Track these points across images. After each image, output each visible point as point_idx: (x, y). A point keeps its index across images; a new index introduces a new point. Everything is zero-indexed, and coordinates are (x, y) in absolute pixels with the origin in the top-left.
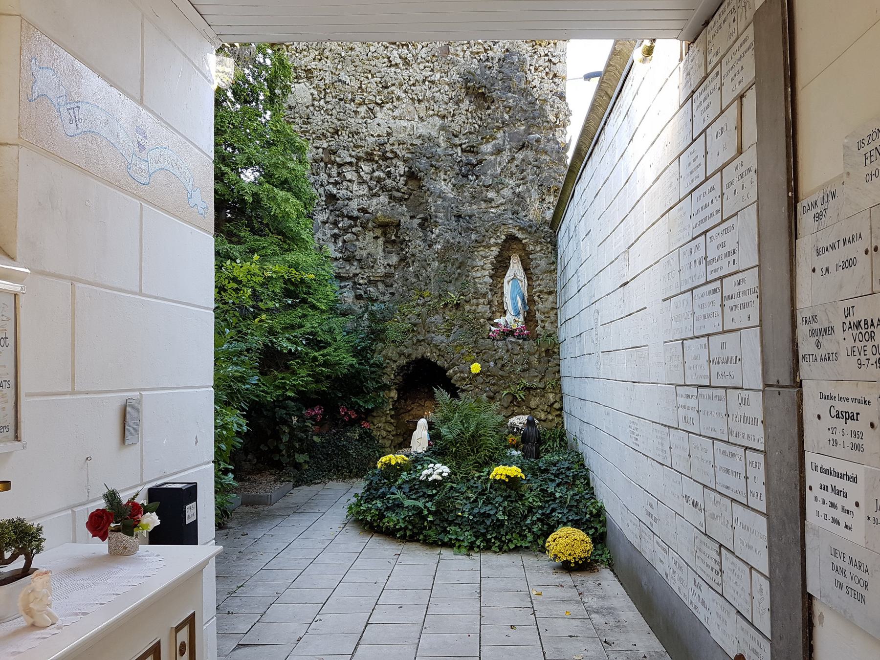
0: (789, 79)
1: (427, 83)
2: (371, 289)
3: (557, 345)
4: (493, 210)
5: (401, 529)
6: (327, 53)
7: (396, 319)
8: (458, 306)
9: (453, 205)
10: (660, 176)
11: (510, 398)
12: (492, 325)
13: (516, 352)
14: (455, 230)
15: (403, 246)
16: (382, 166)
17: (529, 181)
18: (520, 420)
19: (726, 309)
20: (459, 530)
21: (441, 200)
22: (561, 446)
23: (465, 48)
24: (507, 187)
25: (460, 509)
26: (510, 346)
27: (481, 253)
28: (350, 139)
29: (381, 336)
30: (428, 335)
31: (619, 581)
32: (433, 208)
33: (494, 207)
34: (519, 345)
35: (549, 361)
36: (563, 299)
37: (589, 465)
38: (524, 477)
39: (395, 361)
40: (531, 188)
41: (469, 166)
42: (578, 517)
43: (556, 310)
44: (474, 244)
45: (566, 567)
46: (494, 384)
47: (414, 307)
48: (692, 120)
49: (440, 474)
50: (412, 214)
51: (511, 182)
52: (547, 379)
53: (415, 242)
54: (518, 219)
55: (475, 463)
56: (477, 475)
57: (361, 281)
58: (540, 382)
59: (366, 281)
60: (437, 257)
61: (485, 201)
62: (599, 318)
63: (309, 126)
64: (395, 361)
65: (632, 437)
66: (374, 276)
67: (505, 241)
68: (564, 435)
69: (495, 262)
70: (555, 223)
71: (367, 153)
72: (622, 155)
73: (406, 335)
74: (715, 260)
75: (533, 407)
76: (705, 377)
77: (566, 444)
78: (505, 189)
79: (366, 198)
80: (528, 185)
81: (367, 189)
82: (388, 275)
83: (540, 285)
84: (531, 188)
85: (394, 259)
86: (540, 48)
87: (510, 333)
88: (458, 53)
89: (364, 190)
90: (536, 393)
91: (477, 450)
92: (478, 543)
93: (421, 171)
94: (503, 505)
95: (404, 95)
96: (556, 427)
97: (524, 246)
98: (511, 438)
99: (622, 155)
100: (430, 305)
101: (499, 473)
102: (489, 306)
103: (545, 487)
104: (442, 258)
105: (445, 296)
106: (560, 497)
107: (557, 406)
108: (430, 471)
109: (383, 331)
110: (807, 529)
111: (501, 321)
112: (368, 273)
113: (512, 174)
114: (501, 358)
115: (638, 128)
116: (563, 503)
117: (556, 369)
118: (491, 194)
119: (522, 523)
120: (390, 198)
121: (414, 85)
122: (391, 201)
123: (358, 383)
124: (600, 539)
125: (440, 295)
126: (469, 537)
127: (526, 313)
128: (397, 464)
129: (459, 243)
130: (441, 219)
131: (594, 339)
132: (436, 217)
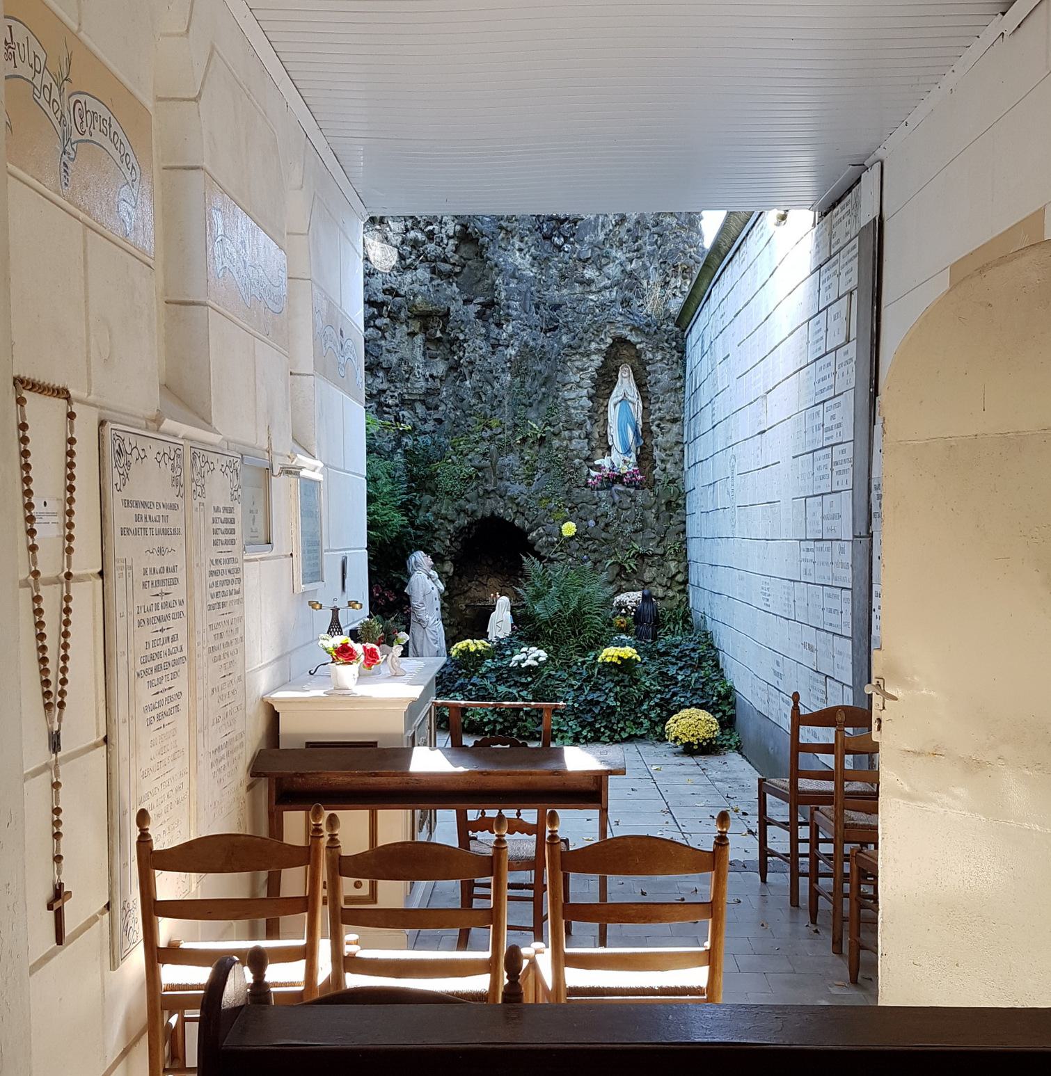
0: (875, 299)
2: (405, 413)
3: (682, 494)
4: (592, 297)
5: (489, 722)
7: (450, 460)
8: (542, 440)
9: (533, 288)
10: (794, 331)
11: (617, 569)
12: (591, 468)
13: (625, 506)
14: (536, 326)
15: (455, 348)
16: (419, 222)
17: (646, 254)
18: (631, 598)
19: (834, 472)
20: (562, 720)
21: (515, 281)
22: (684, 630)
24: (614, 261)
25: (561, 698)
26: (617, 498)
27: (577, 364)
29: (428, 485)
31: (748, 761)
32: (503, 294)
33: (594, 292)
34: (630, 496)
35: (671, 517)
36: (692, 432)
37: (719, 644)
38: (639, 660)
39: (452, 522)
40: (648, 264)
41: (554, 222)
42: (704, 701)
43: (681, 446)
44: (567, 351)
45: (689, 750)
46: (595, 551)
47: (477, 442)
48: (819, 291)
49: (536, 659)
50: (466, 297)
51: (619, 254)
52: (668, 542)
53: (473, 342)
54: (631, 313)
55: (577, 647)
56: (581, 660)
57: (390, 402)
58: (658, 546)
59: (397, 401)
60: (510, 368)
61: (581, 283)
62: (736, 466)
64: (452, 522)
65: (763, 598)
66: (409, 394)
67: (611, 346)
68: (689, 615)
69: (596, 376)
70: (685, 318)
72: (763, 285)
73: (468, 483)
74: (829, 429)
75: (648, 580)
76: (818, 532)
77: (691, 626)
78: (611, 265)
79: (395, 273)
80: (645, 259)
82: (429, 392)
83: (660, 409)
84: (648, 264)
85: (440, 368)
87: (618, 479)
90: (652, 562)
91: (579, 631)
92: (584, 733)
93: (483, 236)
94: (615, 690)
96: (679, 606)
97: (638, 354)
98: (618, 620)
99: (763, 285)
100: (500, 440)
101: (609, 654)
102: (587, 440)
103: (665, 670)
104: (518, 369)
105: (524, 426)
106: (682, 680)
107: (680, 578)
108: (524, 656)
109: (432, 476)
110: (872, 640)
111: (605, 462)
112: (401, 388)
113: (621, 242)
114: (605, 515)
115: (777, 267)
116: (685, 687)
118: (590, 273)
119: (637, 710)
120: (433, 272)
122: (434, 276)
123: (398, 552)
124: (728, 723)
125: (516, 425)
126: (574, 727)
127: (639, 450)
128: (477, 651)
129: (543, 347)
130: (516, 310)
131: (730, 491)
132: (509, 307)
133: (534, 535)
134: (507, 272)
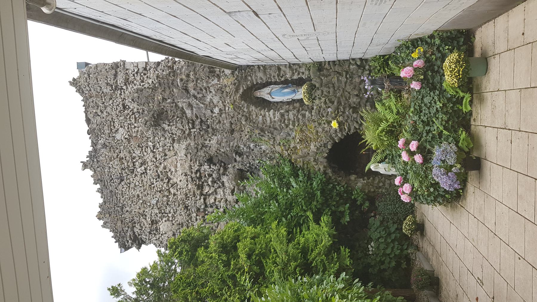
1: (155, 150)
3: (314, 63)
6: (141, 211)
21: (222, 144)
23: (133, 126)
27: (254, 117)
28: (190, 199)
63: (184, 224)
70: (234, 68)
71: (198, 189)
79: (225, 190)
81: (220, 189)
86: (130, 80)
88: (136, 131)
89: (220, 191)
95: (163, 165)
121: (156, 159)
133: (336, 139)
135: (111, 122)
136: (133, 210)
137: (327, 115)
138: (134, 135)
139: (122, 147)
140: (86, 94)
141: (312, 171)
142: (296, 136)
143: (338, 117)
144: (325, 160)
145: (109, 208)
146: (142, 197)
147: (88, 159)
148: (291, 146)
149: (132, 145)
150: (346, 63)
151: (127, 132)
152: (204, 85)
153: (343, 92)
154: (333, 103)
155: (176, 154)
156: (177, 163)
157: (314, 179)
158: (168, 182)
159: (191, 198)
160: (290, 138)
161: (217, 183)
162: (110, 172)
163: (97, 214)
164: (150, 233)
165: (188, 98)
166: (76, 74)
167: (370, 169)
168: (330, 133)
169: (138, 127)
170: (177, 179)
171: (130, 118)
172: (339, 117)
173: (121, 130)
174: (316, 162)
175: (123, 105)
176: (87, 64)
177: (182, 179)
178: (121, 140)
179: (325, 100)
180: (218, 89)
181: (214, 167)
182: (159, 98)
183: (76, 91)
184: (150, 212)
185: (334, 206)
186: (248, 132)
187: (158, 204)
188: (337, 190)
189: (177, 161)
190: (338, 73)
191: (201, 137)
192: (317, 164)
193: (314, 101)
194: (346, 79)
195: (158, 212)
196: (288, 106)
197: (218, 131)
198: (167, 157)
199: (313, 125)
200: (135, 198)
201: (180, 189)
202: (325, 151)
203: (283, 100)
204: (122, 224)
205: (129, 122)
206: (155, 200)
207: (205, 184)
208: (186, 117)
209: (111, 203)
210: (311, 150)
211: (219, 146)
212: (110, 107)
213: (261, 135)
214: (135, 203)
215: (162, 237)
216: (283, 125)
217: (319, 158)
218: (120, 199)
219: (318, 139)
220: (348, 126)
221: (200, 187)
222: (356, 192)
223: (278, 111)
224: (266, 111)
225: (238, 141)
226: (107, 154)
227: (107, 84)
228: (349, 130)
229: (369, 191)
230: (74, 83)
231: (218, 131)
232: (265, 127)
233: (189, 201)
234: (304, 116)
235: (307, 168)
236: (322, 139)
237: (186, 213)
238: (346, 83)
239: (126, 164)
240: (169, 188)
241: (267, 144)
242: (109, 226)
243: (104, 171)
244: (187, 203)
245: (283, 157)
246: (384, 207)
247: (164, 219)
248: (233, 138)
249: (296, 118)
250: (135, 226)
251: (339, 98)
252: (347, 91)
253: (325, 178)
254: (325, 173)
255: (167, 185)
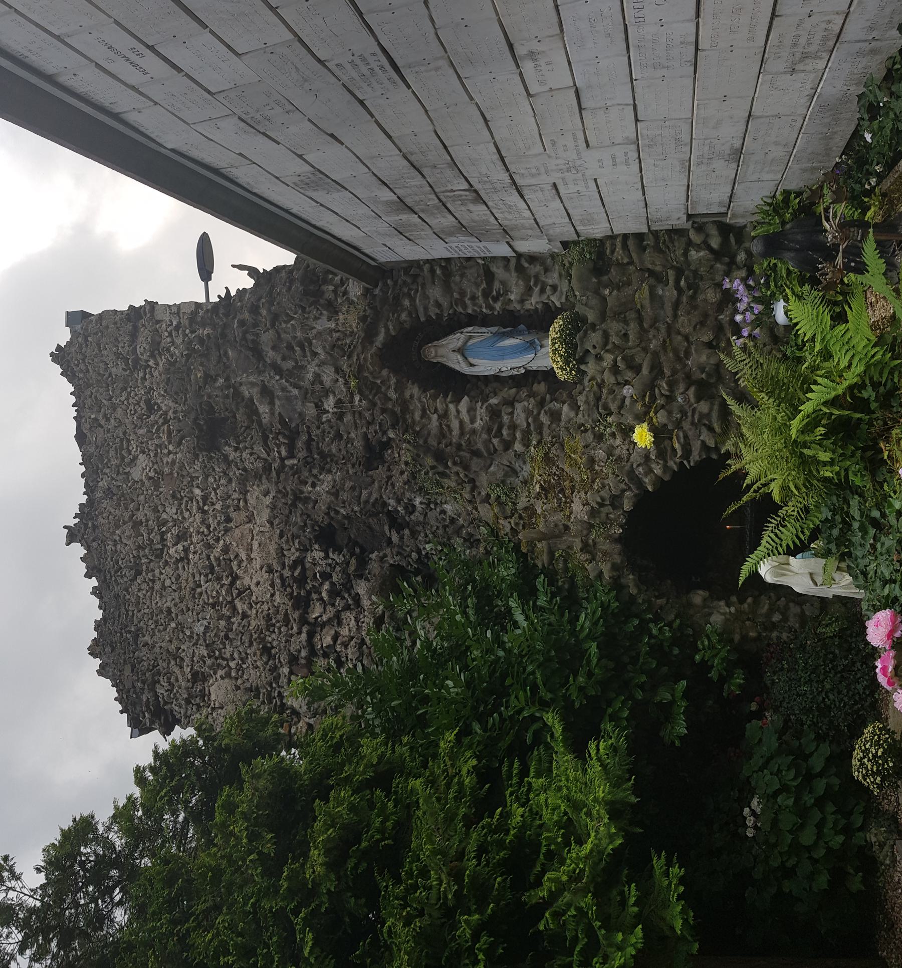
1: (206, 508)
6: (172, 648)
21: (341, 493)
23: (165, 451)
28: (276, 630)
30: (573, 529)
63: (261, 690)
71: (295, 607)
79: (361, 616)
81: (348, 613)
86: (163, 345)
88: (170, 461)
89: (349, 618)
95: (221, 542)
117: (631, 243)
121: (208, 527)
133: (647, 480)
134: (333, 502)
135: (122, 440)
136: (156, 643)
137: (621, 407)
138: (167, 470)
139: (142, 498)
140: (80, 379)
141: (578, 579)
142: (532, 476)
143: (652, 414)
144: (618, 547)
145: (111, 633)
146: (177, 615)
147: (77, 520)
148: (520, 506)
149: (161, 493)
150: (676, 244)
151: (153, 464)
152: (298, 334)
153: (669, 335)
154: (637, 369)
155: (250, 519)
156: (252, 540)
157: (585, 604)
158: (232, 584)
159: (279, 628)
160: (517, 482)
161: (343, 598)
162: (116, 552)
163: (89, 643)
164: (188, 701)
165: (260, 373)
166: (64, 336)
167: (755, 576)
168: (629, 464)
169: (176, 453)
170: (251, 578)
171: (158, 430)
172: (656, 413)
173: (142, 460)
174: (588, 552)
175: (148, 402)
176: (85, 315)
177: (262, 580)
178: (141, 480)
179: (615, 361)
180: (334, 346)
181: (335, 557)
182: (199, 375)
183: (62, 374)
184: (191, 651)
185: (641, 687)
186: (407, 463)
187: (208, 634)
188: (651, 636)
189: (253, 536)
190: (652, 273)
191: (293, 475)
192: (594, 559)
193: (583, 367)
194: (675, 292)
195: (206, 655)
196: (514, 390)
197: (335, 459)
198: (232, 525)
199: (579, 441)
200: (163, 617)
201: (256, 604)
202: (615, 520)
203: (500, 371)
204: (132, 672)
205: (156, 441)
206: (201, 625)
207: (315, 596)
208: (260, 423)
209: (116, 622)
210: (573, 516)
211: (333, 498)
212: (123, 406)
213: (438, 473)
214: (161, 628)
215: (214, 714)
216: (495, 441)
217: (598, 540)
218: (133, 614)
219: (593, 482)
220: (682, 440)
221: (302, 603)
222: (706, 643)
223: (485, 400)
224: (449, 399)
225: (381, 488)
226: (113, 511)
227: (118, 355)
228: (687, 453)
229: (744, 638)
230: (60, 356)
231: (335, 459)
232: (446, 446)
233: (274, 636)
234: (555, 416)
235: (566, 569)
236: (606, 482)
237: (267, 663)
238: (676, 305)
239: (145, 536)
240: (233, 600)
241: (455, 498)
242: (111, 673)
243: (106, 550)
244: (270, 639)
245: (497, 536)
246: (790, 686)
247: (220, 673)
248: (369, 479)
249: (534, 421)
250: (159, 682)
251: (655, 354)
252: (679, 333)
253: (617, 600)
254: (617, 585)
255: (229, 592)
